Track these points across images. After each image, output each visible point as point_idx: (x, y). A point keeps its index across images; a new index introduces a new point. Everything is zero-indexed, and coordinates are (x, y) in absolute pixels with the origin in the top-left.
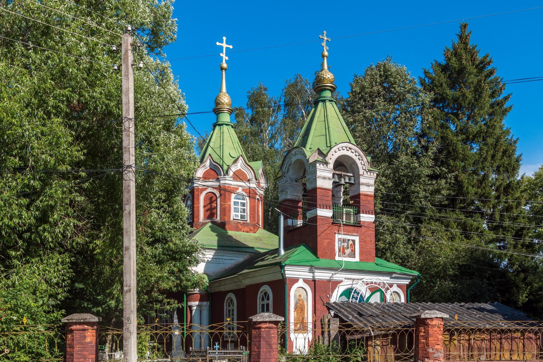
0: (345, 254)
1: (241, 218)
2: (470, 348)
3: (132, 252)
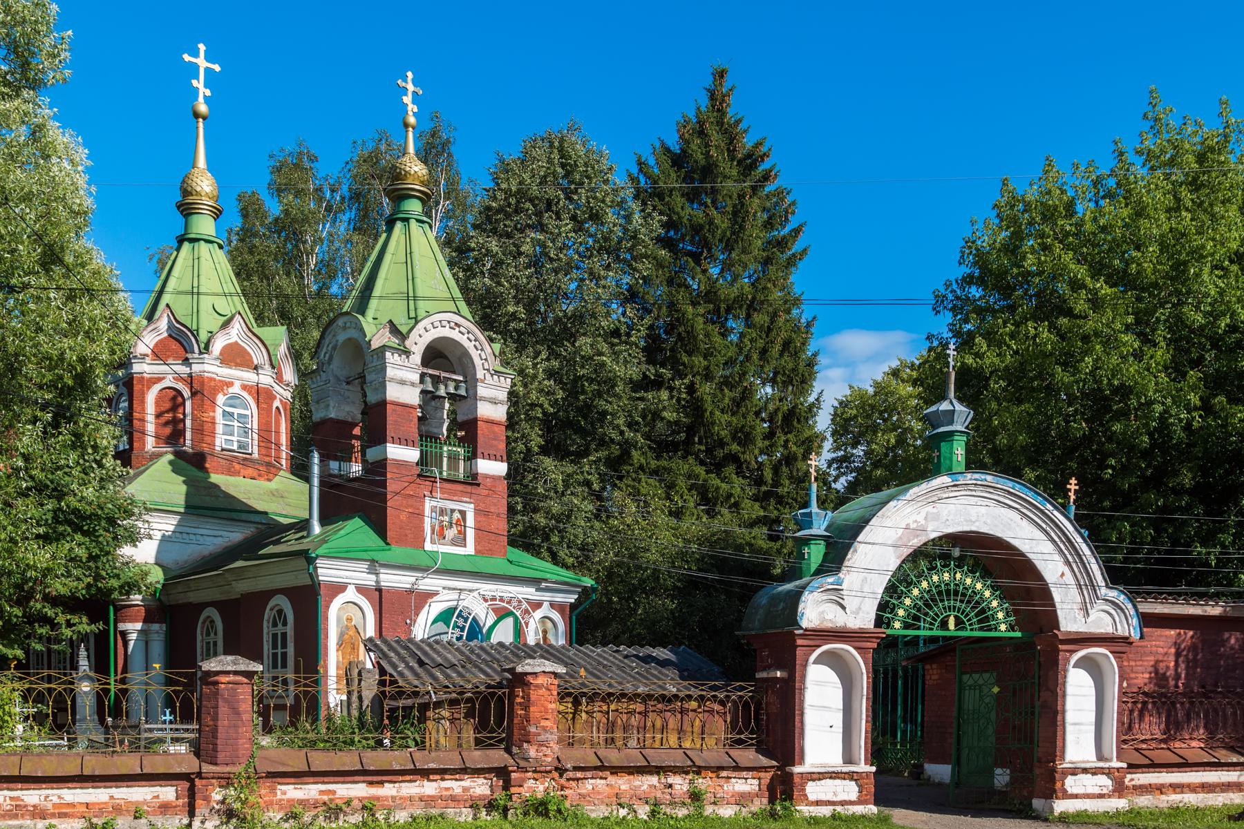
1: (240, 447)
2: (611, 727)
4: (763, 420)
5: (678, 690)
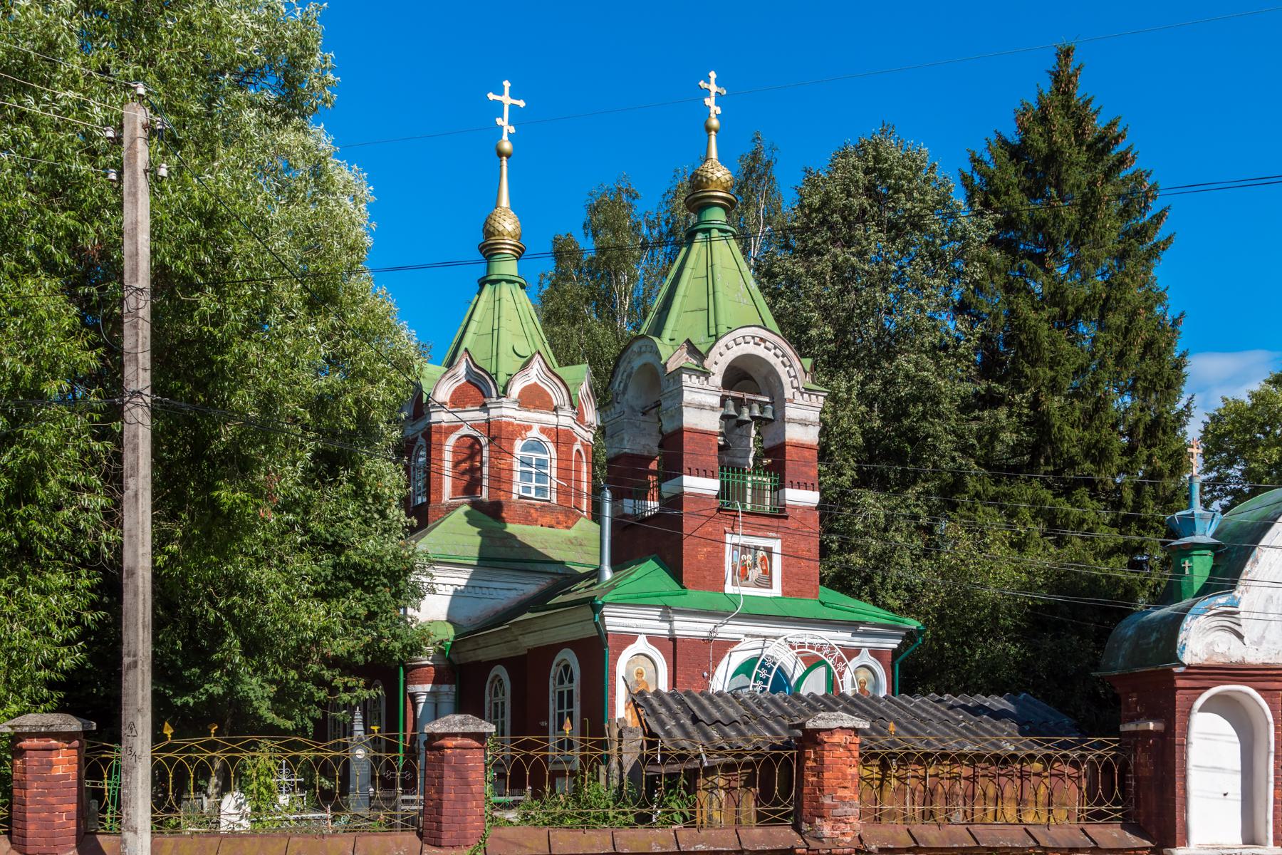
0: (747, 579)
2: (929, 796)
3: (141, 580)
4: (1121, 434)
5: (1017, 749)
